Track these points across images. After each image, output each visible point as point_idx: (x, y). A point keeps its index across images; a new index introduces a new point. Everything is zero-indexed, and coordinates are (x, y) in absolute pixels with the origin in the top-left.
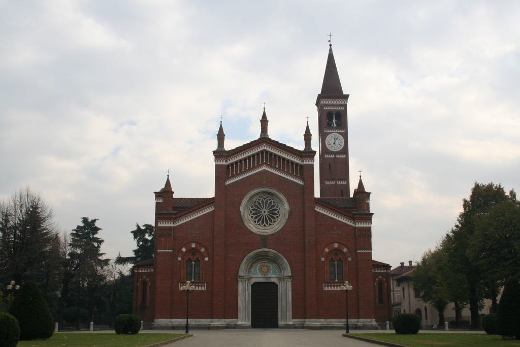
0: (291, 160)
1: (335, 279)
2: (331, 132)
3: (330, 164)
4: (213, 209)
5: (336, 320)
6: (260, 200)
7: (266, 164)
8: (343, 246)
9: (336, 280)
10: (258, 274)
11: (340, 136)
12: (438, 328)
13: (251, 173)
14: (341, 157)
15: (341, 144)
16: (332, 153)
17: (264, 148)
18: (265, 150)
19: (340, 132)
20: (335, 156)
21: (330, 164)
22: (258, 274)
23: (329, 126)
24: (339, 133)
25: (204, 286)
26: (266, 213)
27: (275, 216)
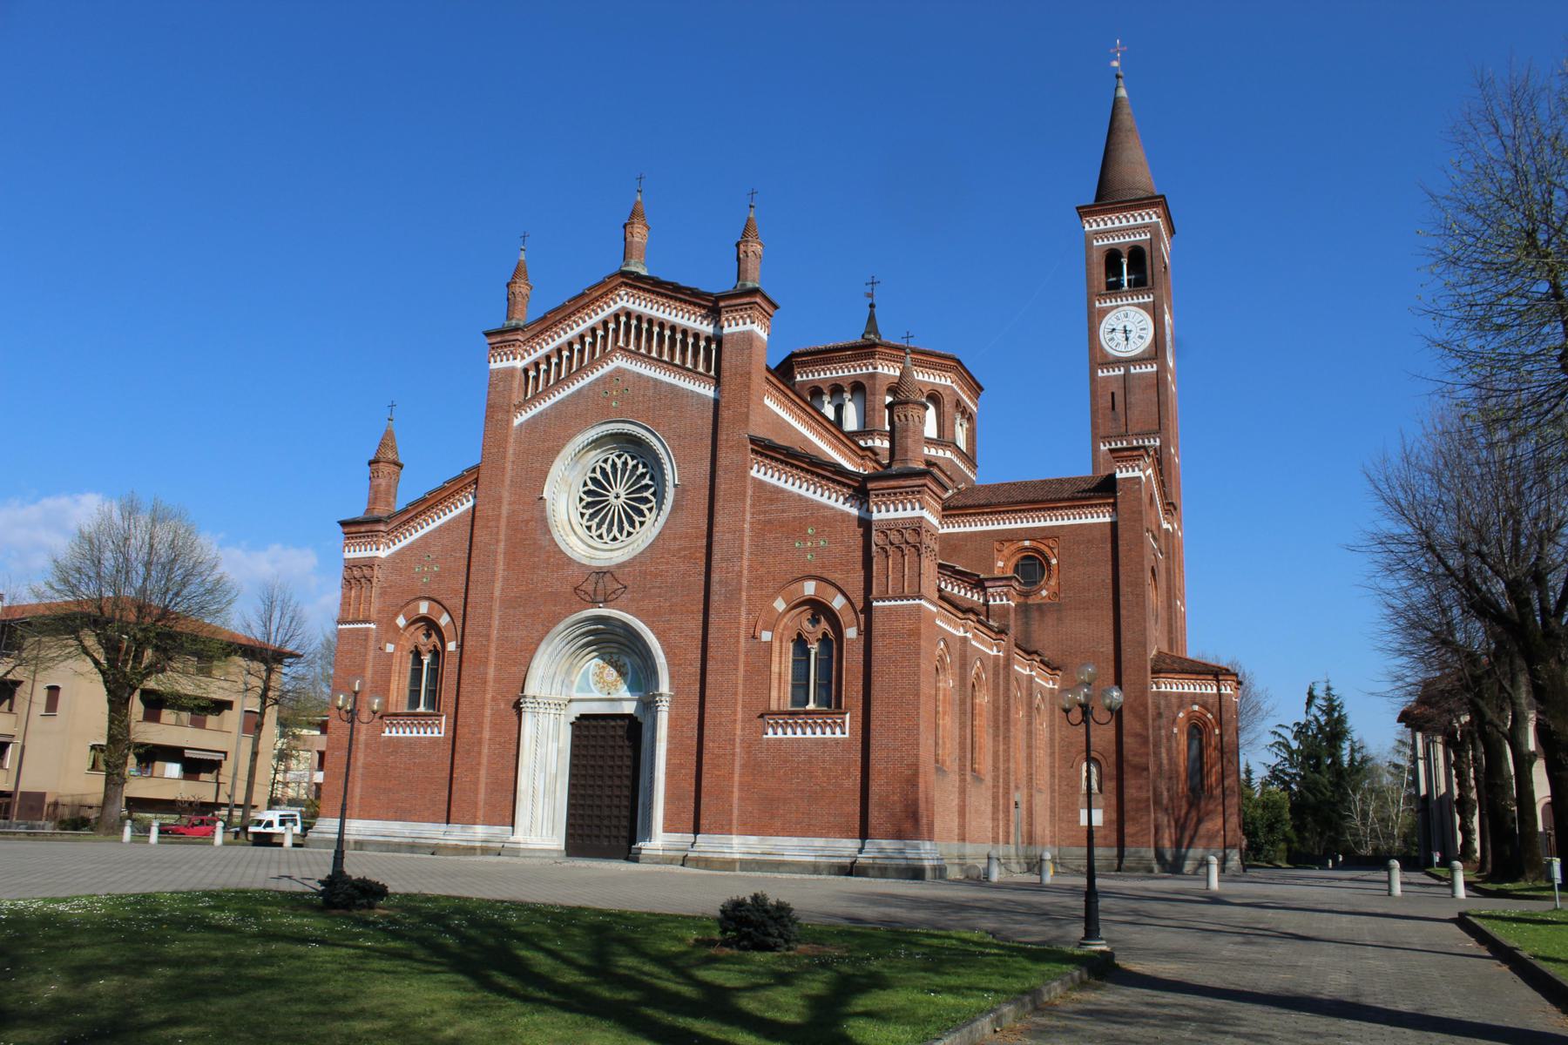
0: (692, 329)
1: (807, 703)
2: (1114, 303)
3: (1113, 394)
4: (471, 504)
5: (795, 841)
6: (606, 461)
7: (625, 350)
8: (831, 590)
9: (811, 706)
10: (592, 691)
11: (1142, 312)
12: (1245, 868)
13: (577, 386)
14: (1144, 370)
15: (1143, 333)
16: (1118, 362)
17: (621, 304)
18: (623, 308)
19: (1141, 300)
20: (1127, 371)
21: (1113, 394)
22: (592, 691)
23: (1114, 287)
24: (1139, 305)
25: (842, 726)
26: (623, 496)
27: (642, 507)
